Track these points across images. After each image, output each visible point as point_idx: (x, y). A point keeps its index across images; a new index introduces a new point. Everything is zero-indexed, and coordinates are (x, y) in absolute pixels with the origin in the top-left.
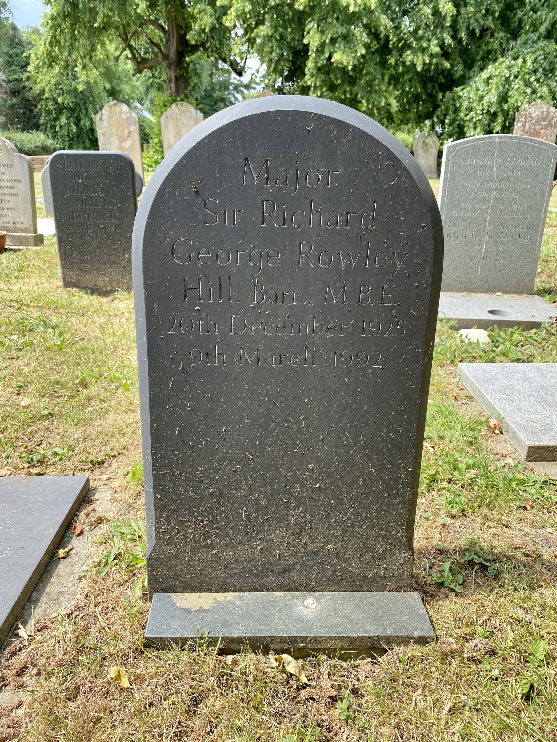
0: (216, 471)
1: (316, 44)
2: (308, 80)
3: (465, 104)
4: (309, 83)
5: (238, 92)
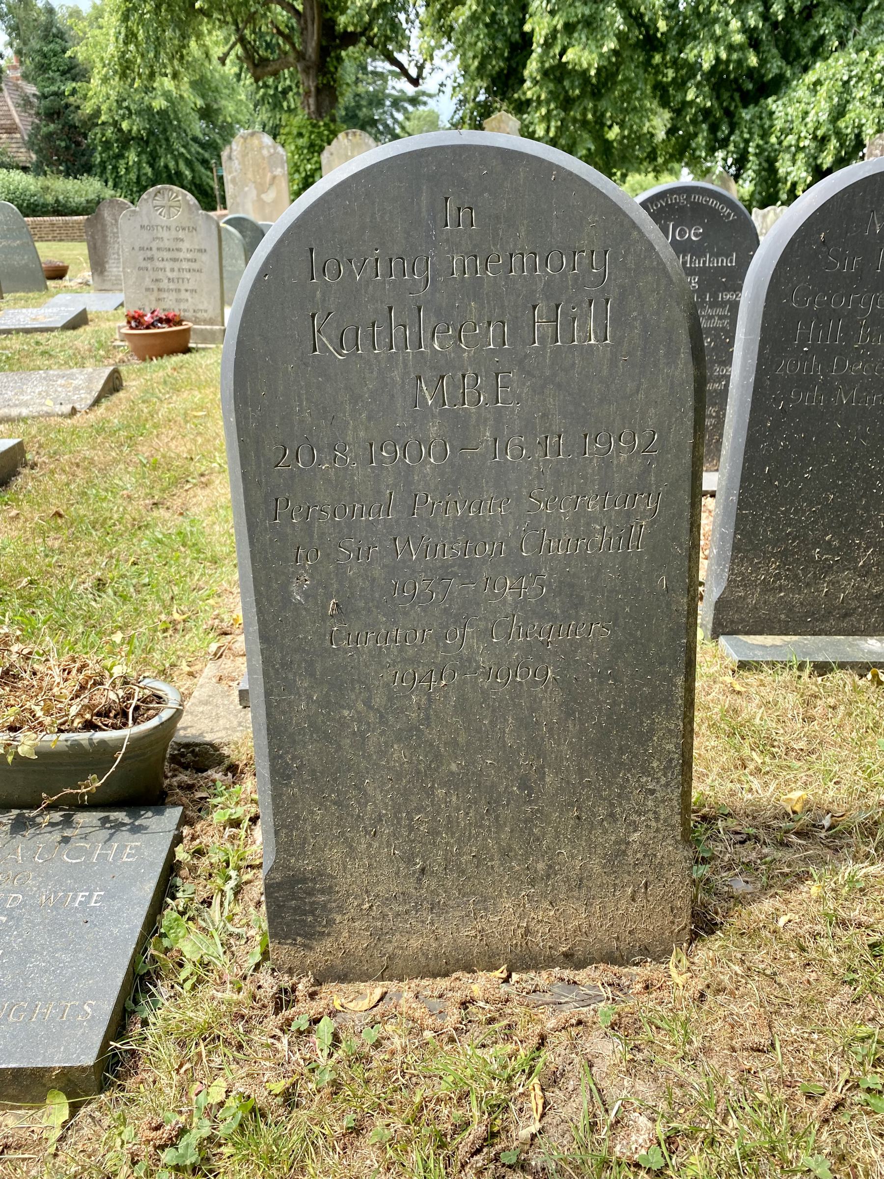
0: (796, 512)
1: (544, 33)
2: (529, 90)
3: (779, 124)
4: (529, 94)
5: (398, 110)
